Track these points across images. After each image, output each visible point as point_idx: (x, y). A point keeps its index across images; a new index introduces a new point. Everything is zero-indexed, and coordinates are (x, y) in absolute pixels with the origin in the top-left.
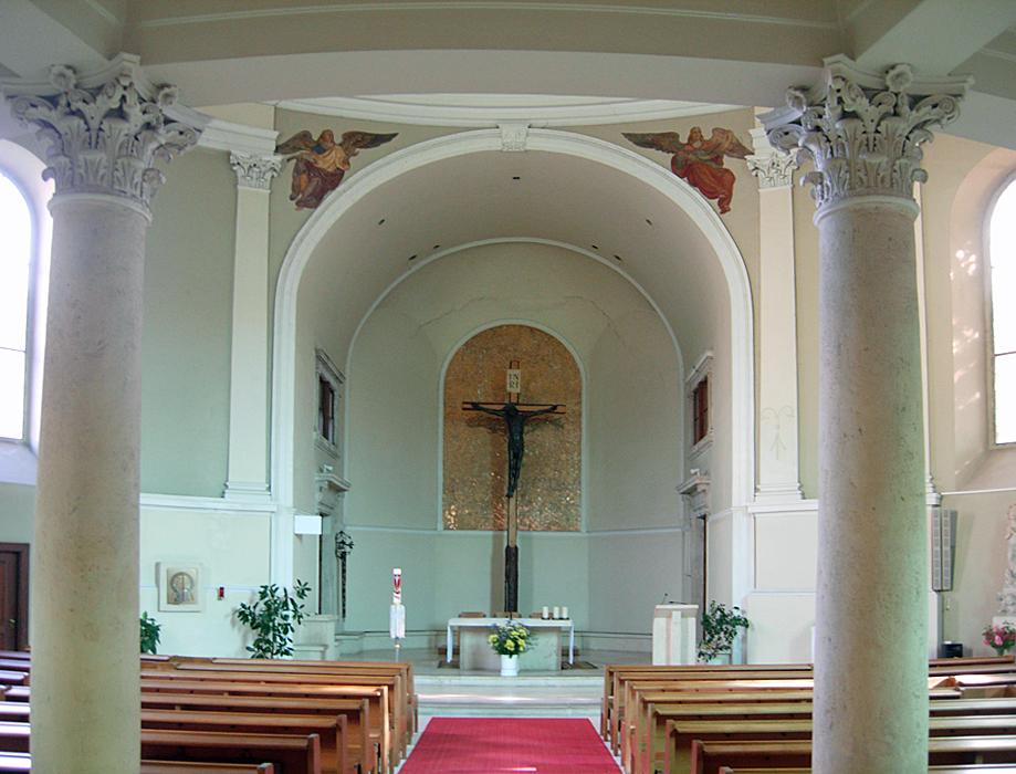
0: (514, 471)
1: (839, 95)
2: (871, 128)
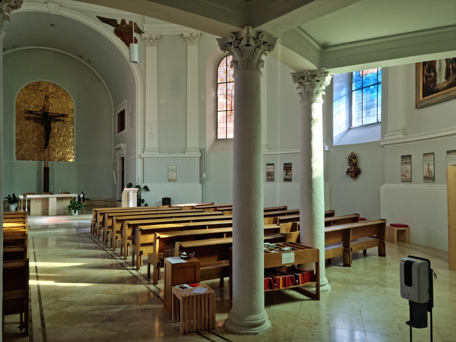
1: (248, 39)
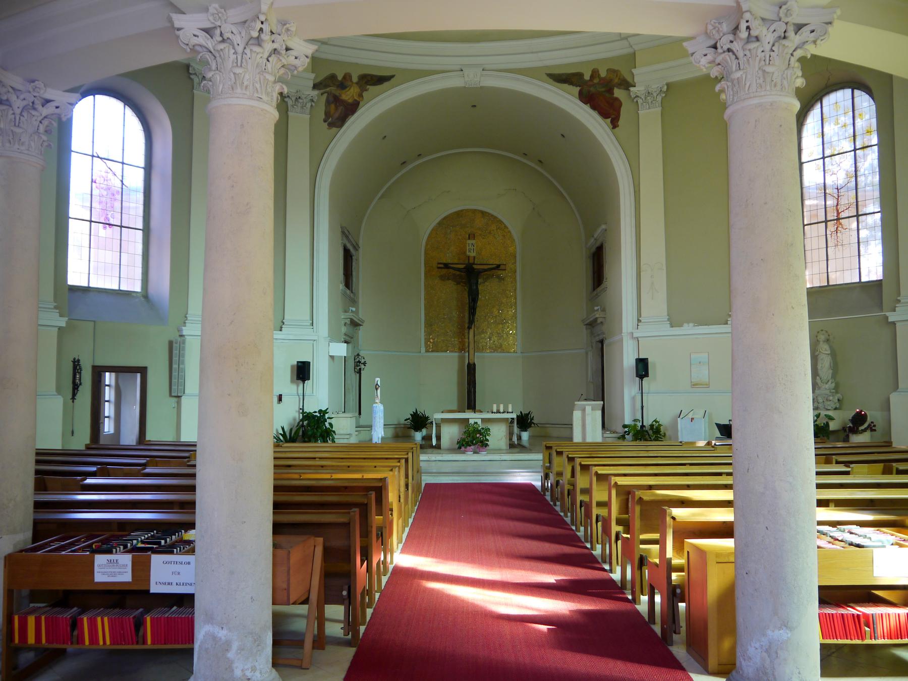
0: (472, 310)
2: (768, 47)
